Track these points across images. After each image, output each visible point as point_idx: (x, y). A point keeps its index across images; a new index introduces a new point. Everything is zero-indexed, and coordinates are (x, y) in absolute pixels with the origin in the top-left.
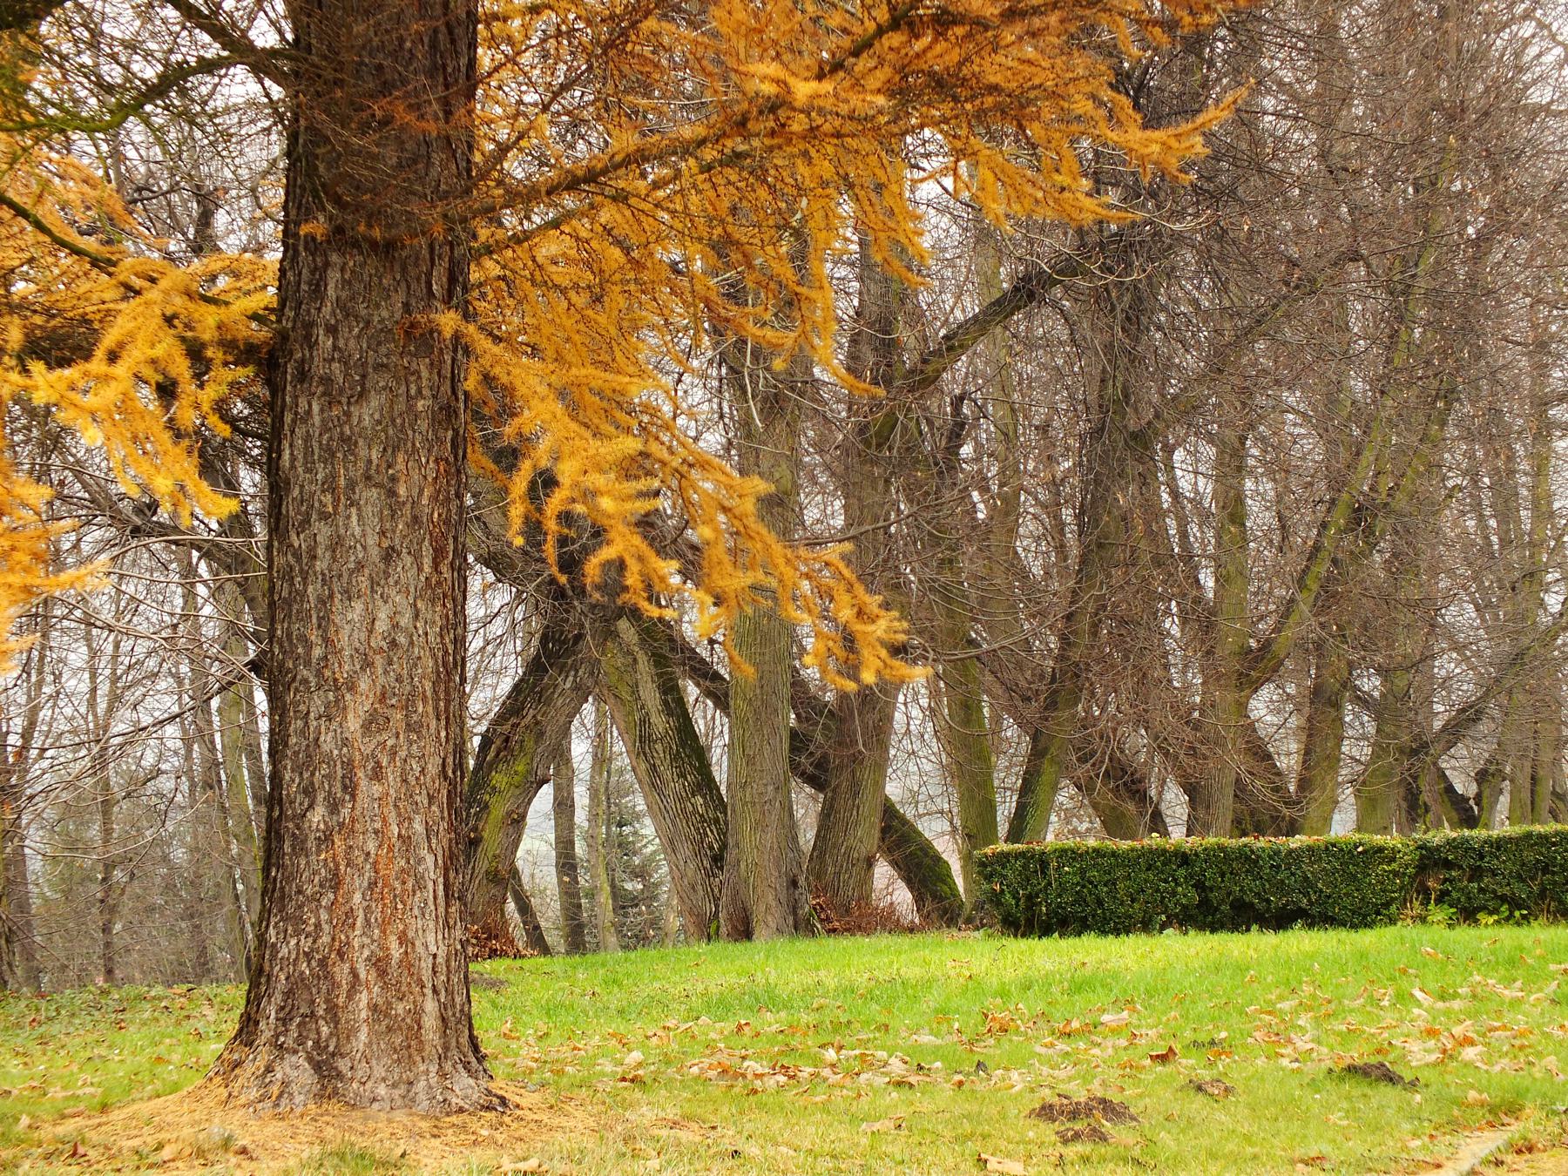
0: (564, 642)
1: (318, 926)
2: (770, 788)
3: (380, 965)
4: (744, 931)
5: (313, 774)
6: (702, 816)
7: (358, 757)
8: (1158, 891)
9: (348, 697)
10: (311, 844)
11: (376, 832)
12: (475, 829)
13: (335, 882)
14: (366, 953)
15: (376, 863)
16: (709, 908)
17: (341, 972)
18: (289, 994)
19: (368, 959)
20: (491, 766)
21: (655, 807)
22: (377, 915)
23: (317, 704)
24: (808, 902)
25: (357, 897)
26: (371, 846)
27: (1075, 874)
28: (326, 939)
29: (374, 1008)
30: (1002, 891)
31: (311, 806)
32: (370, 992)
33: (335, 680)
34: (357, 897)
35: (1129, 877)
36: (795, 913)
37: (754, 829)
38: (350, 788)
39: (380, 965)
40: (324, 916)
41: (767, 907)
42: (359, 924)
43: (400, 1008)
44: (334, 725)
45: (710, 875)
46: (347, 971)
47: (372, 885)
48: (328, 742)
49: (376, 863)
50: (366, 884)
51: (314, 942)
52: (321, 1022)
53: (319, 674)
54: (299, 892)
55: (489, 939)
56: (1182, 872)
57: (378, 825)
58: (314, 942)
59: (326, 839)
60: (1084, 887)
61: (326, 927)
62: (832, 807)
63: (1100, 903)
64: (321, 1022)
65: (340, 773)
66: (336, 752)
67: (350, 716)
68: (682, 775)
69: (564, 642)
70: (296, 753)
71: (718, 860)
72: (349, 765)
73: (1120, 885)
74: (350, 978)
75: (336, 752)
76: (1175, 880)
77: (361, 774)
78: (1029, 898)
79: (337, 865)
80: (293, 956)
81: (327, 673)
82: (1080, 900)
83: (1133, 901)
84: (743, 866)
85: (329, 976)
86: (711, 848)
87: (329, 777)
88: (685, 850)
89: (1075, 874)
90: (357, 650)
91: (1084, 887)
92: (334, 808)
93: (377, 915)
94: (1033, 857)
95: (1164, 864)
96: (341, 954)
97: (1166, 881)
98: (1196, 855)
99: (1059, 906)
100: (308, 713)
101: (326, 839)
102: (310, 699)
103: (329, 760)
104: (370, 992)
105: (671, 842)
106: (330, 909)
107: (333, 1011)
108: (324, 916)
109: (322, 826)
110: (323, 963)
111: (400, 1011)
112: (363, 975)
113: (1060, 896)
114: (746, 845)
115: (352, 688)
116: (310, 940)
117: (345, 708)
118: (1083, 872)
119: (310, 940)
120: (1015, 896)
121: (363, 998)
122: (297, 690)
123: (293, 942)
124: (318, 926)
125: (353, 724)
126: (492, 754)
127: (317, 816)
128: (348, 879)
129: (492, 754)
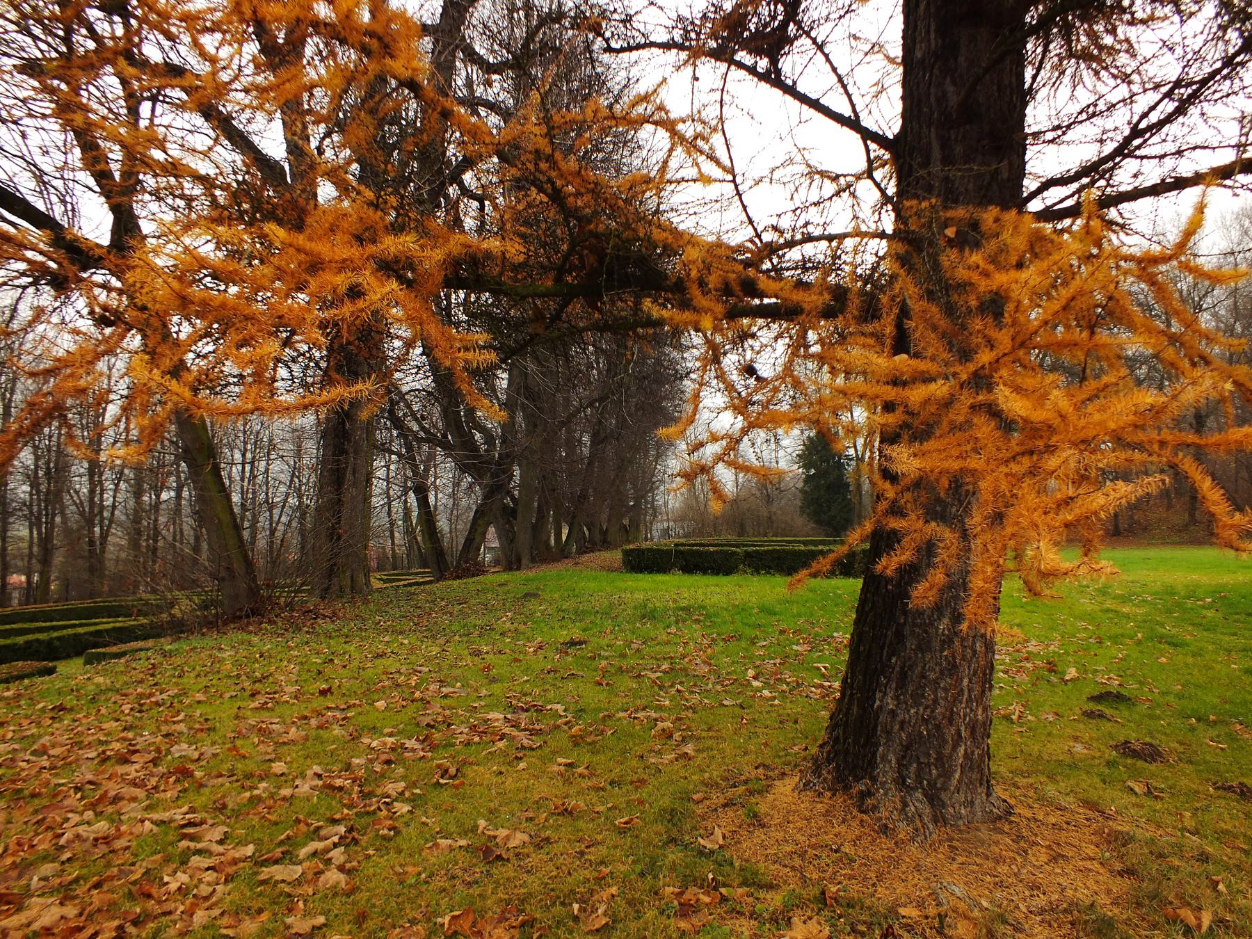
1: (935, 701)
10: (936, 645)
13: (953, 668)
29: (966, 755)
34: (966, 681)
40: (941, 694)
54: (924, 677)
58: (933, 712)
79: (954, 658)
96: (951, 722)
106: (946, 690)
107: (940, 758)
108: (941, 694)
121: (961, 750)
124: (935, 701)
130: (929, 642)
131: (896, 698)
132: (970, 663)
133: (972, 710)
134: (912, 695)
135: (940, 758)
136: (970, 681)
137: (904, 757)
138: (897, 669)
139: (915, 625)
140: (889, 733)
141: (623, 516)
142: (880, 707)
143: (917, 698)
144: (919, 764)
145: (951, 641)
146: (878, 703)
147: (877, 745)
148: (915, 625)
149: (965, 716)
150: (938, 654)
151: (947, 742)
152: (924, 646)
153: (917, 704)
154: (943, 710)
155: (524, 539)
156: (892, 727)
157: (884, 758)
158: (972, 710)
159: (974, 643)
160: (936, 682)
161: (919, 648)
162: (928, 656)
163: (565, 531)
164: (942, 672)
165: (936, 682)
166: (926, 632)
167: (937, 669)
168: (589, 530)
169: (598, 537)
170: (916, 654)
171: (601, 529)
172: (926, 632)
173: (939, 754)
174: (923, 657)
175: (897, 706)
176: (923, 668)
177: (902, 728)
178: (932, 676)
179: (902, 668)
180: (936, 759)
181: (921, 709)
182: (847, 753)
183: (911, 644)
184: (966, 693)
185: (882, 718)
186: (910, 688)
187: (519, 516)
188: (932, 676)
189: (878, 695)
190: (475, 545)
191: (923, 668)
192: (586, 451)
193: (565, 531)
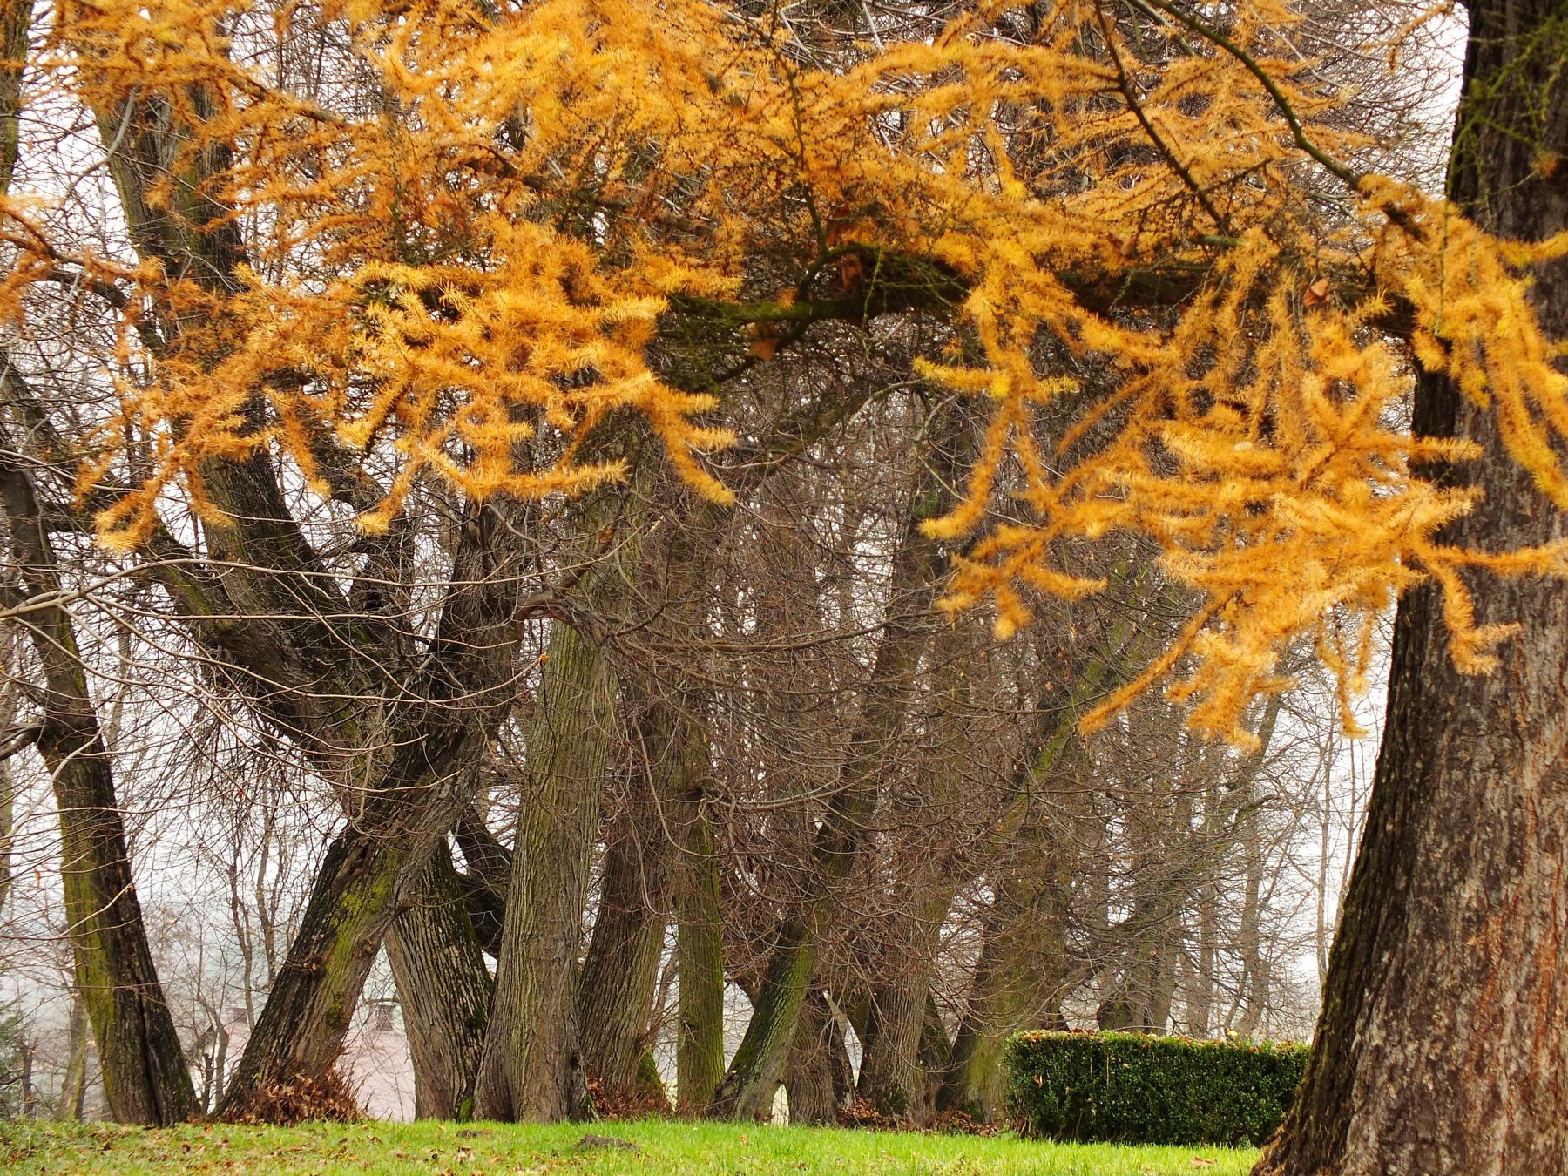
0: (442, 741)
1: (1452, 1029)
2: (561, 944)
3: (1526, 1085)
4: (507, 1112)
5: (1469, 838)
6: (456, 971)
7: (1530, 821)
8: (1236, 1101)
9: (1528, 746)
10: (1456, 927)
11: (1544, 916)
12: (317, 960)
13: (1483, 973)
14: (1513, 1068)
15: (1537, 956)
16: (459, 1083)
17: (1477, 1090)
18: (1397, 1113)
19: (1515, 1076)
20: (342, 884)
21: (400, 955)
22: (1530, 1021)
23: (1484, 754)
24: (586, 1087)
25: (1510, 997)
26: (1535, 934)
27: (1136, 1072)
28: (1459, 1046)
29: (1511, 1139)
30: (1045, 1085)
31: (1462, 879)
32: (1511, 1118)
33: (1515, 724)
34: (1510, 997)
35: (1202, 1082)
36: (570, 1099)
37: (535, 992)
38: (1516, 859)
39: (1526, 1085)
40: (1462, 1016)
41: (539, 1083)
42: (1507, 1031)
43: (1540, 1142)
44: (1506, 780)
45: (462, 1042)
46: (1484, 1089)
47: (1530, 982)
48: (1493, 795)
49: (1537, 956)
50: (1522, 981)
51: (1445, 1048)
52: (1443, 1152)
53: (1493, 714)
54: (1431, 984)
55: (326, 1096)
56: (1267, 1081)
57: (1547, 908)
58: (1445, 1048)
59: (1477, 921)
60: (1145, 1088)
61: (1463, 1032)
62: (596, 974)
63: (1164, 1110)
64: (1443, 1152)
65: (1506, 842)
66: (1504, 813)
67: (1528, 771)
68: (436, 919)
69: (442, 741)
70: (1447, 812)
71: (474, 1024)
72: (1518, 830)
73: (1190, 1090)
74: (1489, 1099)
75: (1504, 813)
76: (1258, 1090)
77: (1532, 842)
78: (1076, 1095)
79: (1488, 954)
80: (1411, 1065)
81: (1503, 714)
82: (1140, 1104)
83: (1205, 1111)
84: (515, 1036)
85: (1461, 1097)
86: (466, 1011)
87: (1492, 843)
88: (433, 1010)
89: (1136, 1072)
90: (1546, 689)
91: (1145, 1088)
92: (1493, 881)
93: (1530, 1021)
94: (1086, 1047)
95: (1247, 1069)
96: (1479, 1068)
97: (1246, 1090)
98: (1287, 1061)
99: (1114, 1109)
100: (1471, 762)
101: (1477, 921)
102: (1476, 745)
103: (1492, 821)
104: (1511, 1118)
105: (416, 998)
106: (1470, 1009)
107: (1458, 1134)
108: (1462, 1016)
109: (1474, 904)
110: (1453, 1076)
111: (1540, 1147)
112: (1504, 1096)
113: (1115, 1097)
114: (521, 1009)
115: (1535, 733)
116: (1439, 1046)
117: (1523, 758)
118: (1146, 1071)
119: (1439, 1046)
120: (1060, 1093)
121: (1501, 1125)
122: (1456, 732)
123: (1411, 1047)
124: (1452, 1029)
125: (1530, 780)
126: (344, 870)
127: (1470, 891)
128: (1501, 973)
129: (344, 870)
130: (1444, 922)
131: (1386, 1024)
132: (1518, 963)
133: (1522, 1053)
134: (1410, 1019)
135: (1458, 1134)
136: (1519, 998)
137: (1390, 1130)
138: (1391, 974)
139: (1421, 891)
140: (1368, 1088)
141: (1066, 972)
142: (1360, 1046)
143: (1421, 1023)
144: (1420, 1142)
145: (1481, 920)
146: (1358, 1038)
147: (1349, 1113)
148: (1421, 891)
149: (1508, 1060)
150: (1458, 943)
151: (1472, 1107)
152: (1435, 929)
153: (1419, 1035)
154: (1465, 1047)
155: (536, 1017)
156: (1374, 1077)
157: (1358, 1130)
158: (1522, 1053)
159: (1528, 927)
160: (1453, 994)
161: (1427, 932)
162: (1441, 947)
163: (737, 1011)
164: (1464, 977)
165: (1453, 994)
166: (1439, 903)
167: (1457, 970)
168: (868, 1034)
169: (909, 1075)
170: (1420, 943)
171: (932, 1032)
172: (1439, 903)
173: (1455, 1126)
174: (1433, 950)
175: (1385, 1040)
176: (1433, 969)
177: (1391, 1079)
178: (1446, 983)
179: (1398, 971)
180: (1451, 1137)
181: (1427, 1043)
182: (1305, 1140)
183: (1415, 926)
184: (1511, 1017)
185: (1365, 1063)
186: (1410, 1008)
187: (517, 915)
188: (1446, 983)
189: (1360, 1023)
190: (324, 1003)
191: (1433, 969)
192: (868, 610)
193: (737, 1011)
